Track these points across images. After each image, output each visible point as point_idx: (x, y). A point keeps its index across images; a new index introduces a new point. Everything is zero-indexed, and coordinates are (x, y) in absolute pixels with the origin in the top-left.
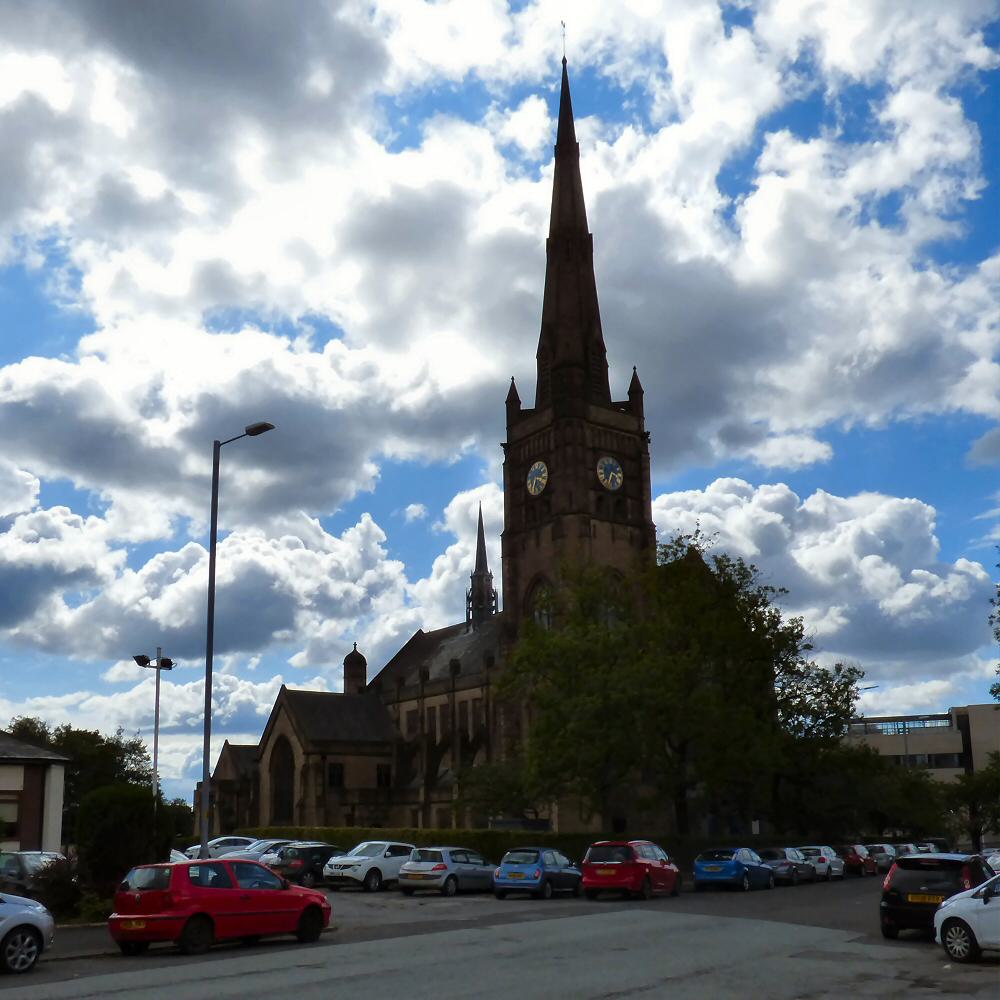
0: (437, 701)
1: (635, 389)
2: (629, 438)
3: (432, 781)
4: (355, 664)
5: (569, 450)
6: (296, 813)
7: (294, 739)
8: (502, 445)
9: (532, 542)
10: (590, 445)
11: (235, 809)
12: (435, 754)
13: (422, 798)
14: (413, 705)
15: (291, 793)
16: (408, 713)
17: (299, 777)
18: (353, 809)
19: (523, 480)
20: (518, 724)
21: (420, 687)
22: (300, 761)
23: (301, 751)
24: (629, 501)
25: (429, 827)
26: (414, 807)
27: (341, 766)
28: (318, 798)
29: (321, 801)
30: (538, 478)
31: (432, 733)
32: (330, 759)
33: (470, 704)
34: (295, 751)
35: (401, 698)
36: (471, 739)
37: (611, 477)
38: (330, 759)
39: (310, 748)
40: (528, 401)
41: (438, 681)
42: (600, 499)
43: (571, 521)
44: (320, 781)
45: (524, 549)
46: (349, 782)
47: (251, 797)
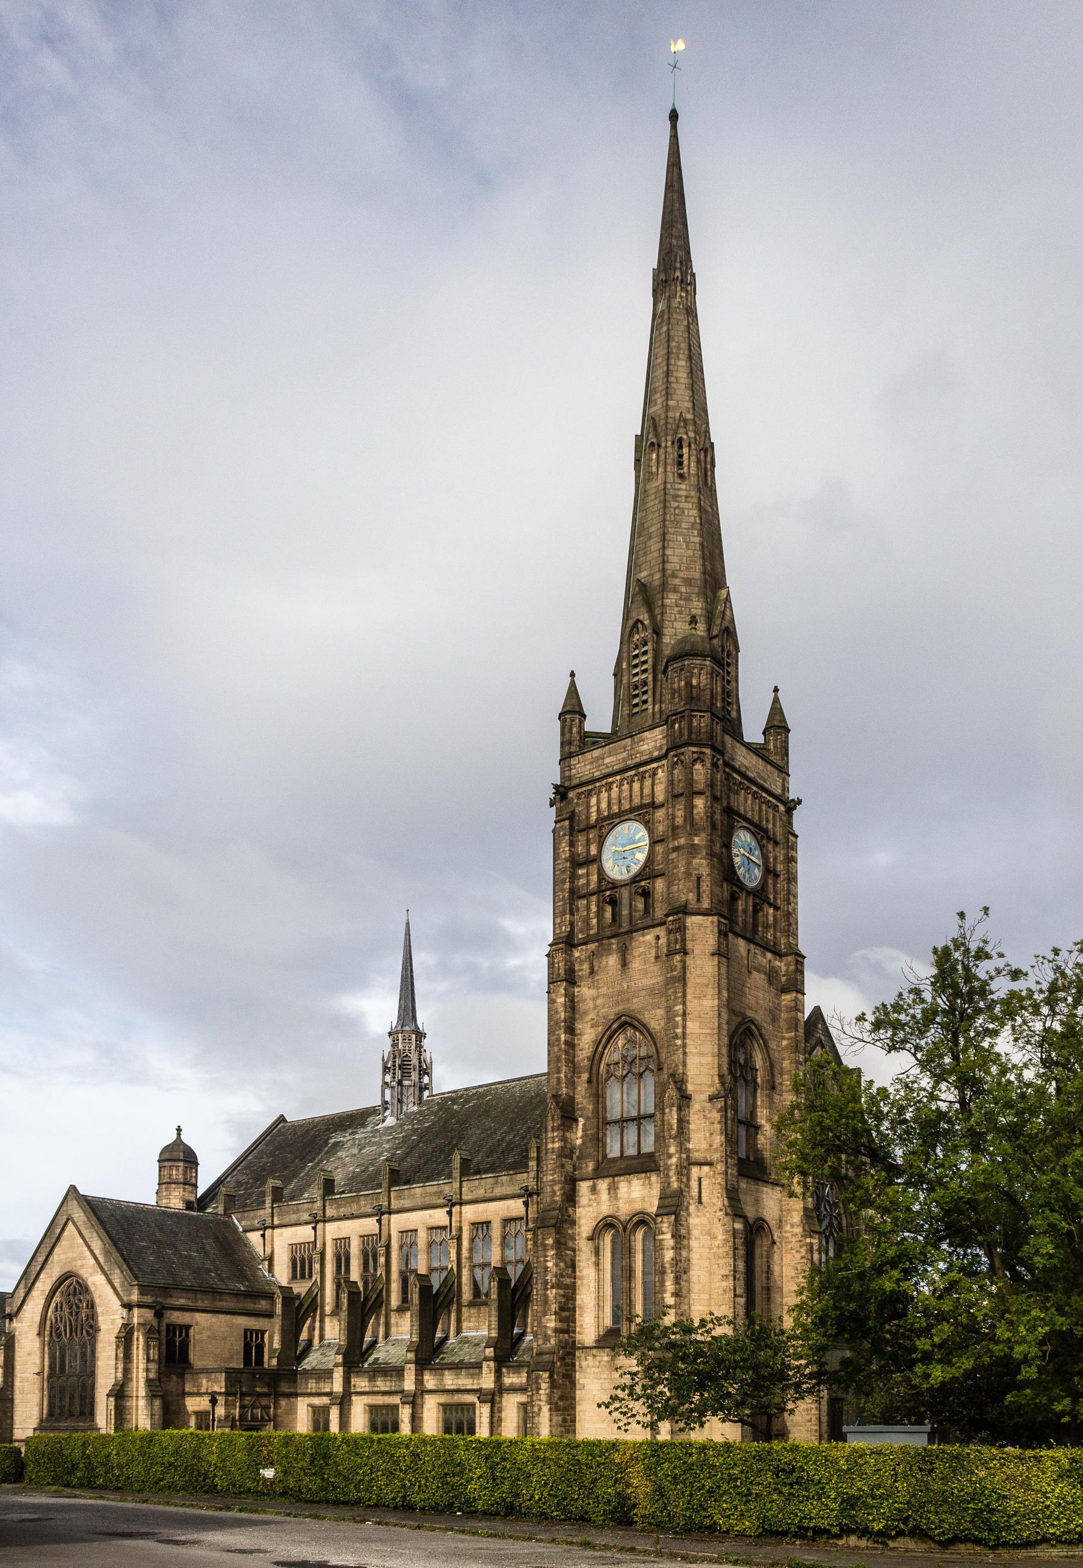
1: (777, 725)
4: (179, 1158)
7: (96, 1282)
9: (612, 961)
13: (337, 1386)
14: (305, 1233)
18: (214, 1402)
19: (593, 851)
20: (573, 1266)
22: (111, 1315)
33: (422, 1237)
35: (276, 1222)
40: (599, 717)
44: (154, 1353)
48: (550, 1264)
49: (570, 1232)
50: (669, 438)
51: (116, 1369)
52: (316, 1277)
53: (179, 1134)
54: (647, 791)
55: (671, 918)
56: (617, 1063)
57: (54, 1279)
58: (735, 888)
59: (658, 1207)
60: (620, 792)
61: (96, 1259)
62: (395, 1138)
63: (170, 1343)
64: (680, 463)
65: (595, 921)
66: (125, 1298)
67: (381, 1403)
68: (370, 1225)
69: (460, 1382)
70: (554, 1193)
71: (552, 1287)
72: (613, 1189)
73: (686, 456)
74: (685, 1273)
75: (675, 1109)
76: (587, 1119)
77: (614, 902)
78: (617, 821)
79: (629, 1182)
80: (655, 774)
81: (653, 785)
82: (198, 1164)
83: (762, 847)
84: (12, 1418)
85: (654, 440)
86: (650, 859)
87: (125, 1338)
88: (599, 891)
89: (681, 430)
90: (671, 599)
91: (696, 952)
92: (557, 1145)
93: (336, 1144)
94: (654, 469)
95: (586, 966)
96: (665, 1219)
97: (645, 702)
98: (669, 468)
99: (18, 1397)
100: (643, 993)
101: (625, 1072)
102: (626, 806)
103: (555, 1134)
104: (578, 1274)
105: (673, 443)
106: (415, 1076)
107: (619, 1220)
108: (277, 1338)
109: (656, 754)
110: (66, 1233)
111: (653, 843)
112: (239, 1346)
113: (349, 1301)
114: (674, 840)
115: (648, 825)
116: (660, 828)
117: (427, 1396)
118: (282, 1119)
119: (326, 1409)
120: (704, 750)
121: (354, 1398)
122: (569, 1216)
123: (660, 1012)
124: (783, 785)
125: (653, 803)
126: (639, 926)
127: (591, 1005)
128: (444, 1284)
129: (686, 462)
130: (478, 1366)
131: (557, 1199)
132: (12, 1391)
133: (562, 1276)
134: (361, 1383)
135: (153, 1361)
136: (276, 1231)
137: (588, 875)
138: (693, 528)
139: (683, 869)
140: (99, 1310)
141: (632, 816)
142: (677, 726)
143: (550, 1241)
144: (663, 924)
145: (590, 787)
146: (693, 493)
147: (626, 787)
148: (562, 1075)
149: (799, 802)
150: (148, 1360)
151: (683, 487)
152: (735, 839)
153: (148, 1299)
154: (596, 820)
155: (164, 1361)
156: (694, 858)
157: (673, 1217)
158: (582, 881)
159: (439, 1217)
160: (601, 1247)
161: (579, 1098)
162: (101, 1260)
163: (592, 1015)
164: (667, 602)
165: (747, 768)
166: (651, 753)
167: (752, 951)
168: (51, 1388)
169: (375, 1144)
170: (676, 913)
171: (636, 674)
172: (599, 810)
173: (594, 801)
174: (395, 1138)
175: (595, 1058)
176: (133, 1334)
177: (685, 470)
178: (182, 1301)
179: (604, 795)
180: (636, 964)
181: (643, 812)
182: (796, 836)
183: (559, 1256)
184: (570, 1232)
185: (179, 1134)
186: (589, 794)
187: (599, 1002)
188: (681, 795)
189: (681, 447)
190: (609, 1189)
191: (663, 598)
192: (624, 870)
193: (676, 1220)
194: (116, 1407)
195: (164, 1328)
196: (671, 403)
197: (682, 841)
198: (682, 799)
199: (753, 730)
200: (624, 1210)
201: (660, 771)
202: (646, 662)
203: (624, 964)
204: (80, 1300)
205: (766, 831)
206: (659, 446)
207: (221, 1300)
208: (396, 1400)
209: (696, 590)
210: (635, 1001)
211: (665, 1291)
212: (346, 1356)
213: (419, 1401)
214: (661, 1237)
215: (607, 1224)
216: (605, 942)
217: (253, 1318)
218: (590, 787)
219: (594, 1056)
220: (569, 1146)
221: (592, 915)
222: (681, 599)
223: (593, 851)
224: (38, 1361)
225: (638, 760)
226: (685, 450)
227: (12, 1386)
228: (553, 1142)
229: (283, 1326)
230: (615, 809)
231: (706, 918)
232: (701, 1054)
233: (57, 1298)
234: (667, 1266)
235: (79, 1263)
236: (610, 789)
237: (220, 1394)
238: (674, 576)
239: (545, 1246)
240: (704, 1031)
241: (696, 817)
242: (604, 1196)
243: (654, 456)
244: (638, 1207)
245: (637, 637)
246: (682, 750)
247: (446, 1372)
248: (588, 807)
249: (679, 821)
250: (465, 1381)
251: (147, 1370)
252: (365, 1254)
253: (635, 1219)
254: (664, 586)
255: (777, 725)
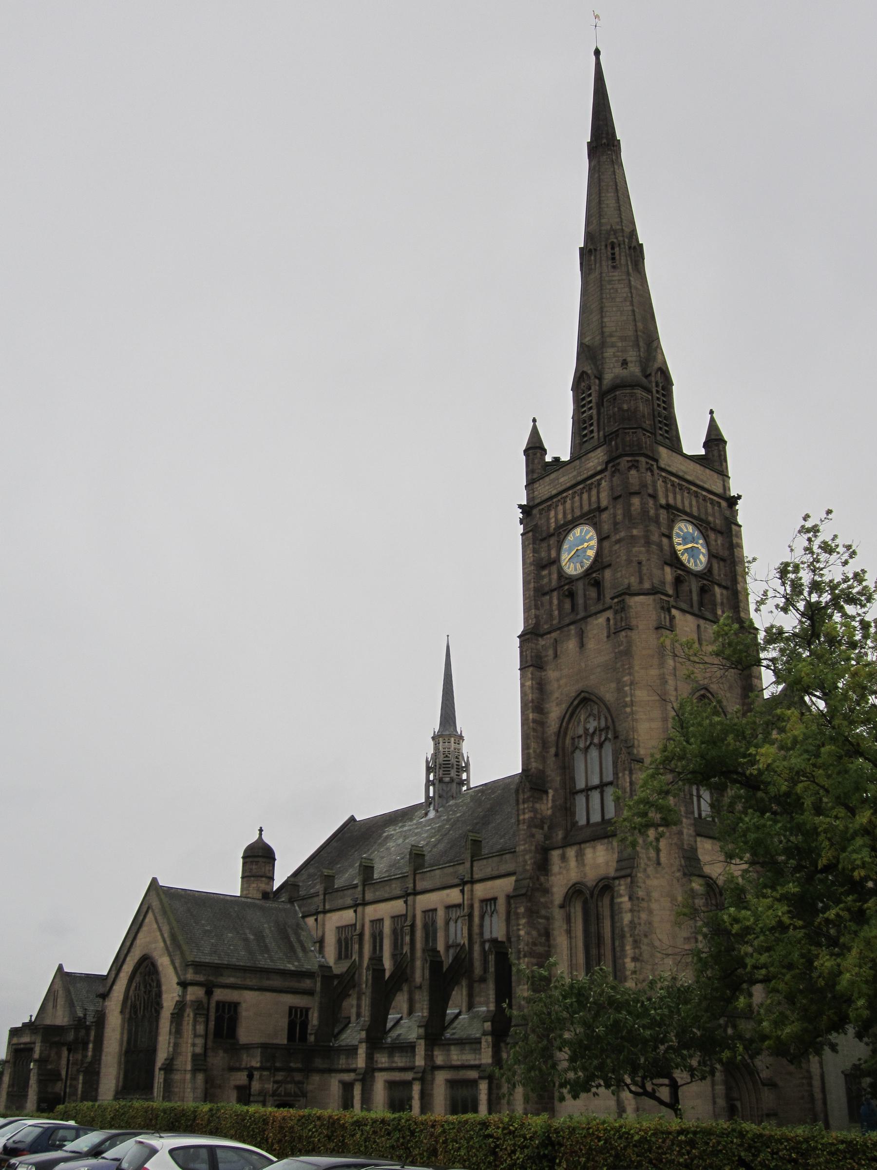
0: (386, 910)
1: (715, 441)
2: (712, 502)
3: (376, 1036)
5: (636, 501)
6: (159, 1077)
7: (164, 962)
8: (520, 506)
9: (571, 645)
10: (663, 501)
11: (64, 1073)
12: (385, 991)
13: (361, 1062)
14: (347, 916)
15: (152, 1051)
16: (339, 929)
17: (168, 1024)
18: (250, 1077)
19: (553, 554)
20: (547, 934)
21: (360, 888)
23: (175, 980)
24: (717, 590)
25: (369, 1110)
26: (348, 1077)
27: (234, 1007)
28: (195, 1056)
29: (200, 1063)
30: (580, 548)
31: (377, 959)
32: (219, 995)
33: (441, 913)
34: (163, 980)
35: (327, 907)
36: (387, 975)
37: (691, 547)
38: (219, 995)
39: (190, 976)
40: (559, 445)
41: (386, 882)
42: (678, 581)
43: (642, 608)
44: (200, 1029)
45: (556, 656)
46: (244, 1035)
47: (90, 1054)
48: (522, 933)
49: (542, 900)
50: (603, 243)
51: (169, 1043)
52: (355, 956)
53: (261, 834)
54: (594, 499)
55: (616, 600)
56: (580, 737)
57: (136, 961)
58: (679, 572)
59: (617, 870)
60: (573, 503)
61: (164, 941)
62: (432, 828)
63: (219, 1019)
64: (613, 259)
65: (556, 613)
66: (182, 977)
67: (398, 1079)
68: (398, 906)
69: (464, 1057)
70: (525, 861)
71: (525, 956)
72: (580, 855)
73: (617, 253)
74: (646, 936)
75: (627, 772)
76: (556, 790)
77: (571, 595)
78: (570, 527)
79: (594, 848)
80: (599, 484)
81: (598, 493)
82: (275, 859)
83: (706, 538)
84: (97, 1090)
85: (592, 247)
86: (598, 554)
87: (177, 1016)
88: (559, 588)
89: (612, 237)
90: (609, 352)
91: (641, 627)
92: (527, 816)
93: (387, 837)
94: (593, 266)
95: (551, 652)
96: (622, 882)
97: (592, 432)
98: (604, 263)
99: (103, 1070)
100: (599, 670)
101: (588, 743)
102: (578, 513)
103: (526, 806)
104: (552, 942)
105: (606, 246)
106: (453, 773)
107: (586, 886)
108: (316, 1015)
109: (599, 468)
110: (147, 920)
111: (601, 540)
112: (284, 1023)
113: (373, 977)
114: (616, 534)
115: (596, 526)
116: (606, 527)
117: (376, 1074)
118: (352, 819)
119: (408, 1084)
120: (637, 458)
121: (376, 1074)
122: (541, 884)
123: (613, 685)
124: (724, 485)
125: (599, 507)
126: (593, 612)
127: (556, 685)
128: (456, 958)
129: (617, 257)
130: (478, 1041)
131: (528, 868)
132: (100, 1064)
133: (534, 944)
134: (382, 1060)
135: (200, 1036)
136: (328, 915)
137: (550, 574)
138: (625, 301)
139: (624, 558)
140: (164, 988)
141: (582, 521)
142: (613, 443)
143: (521, 910)
144: (610, 608)
145: (549, 503)
146: (624, 277)
147: (577, 498)
148: (531, 751)
149: (739, 497)
150: (196, 1036)
151: (616, 274)
152: (676, 530)
153: (201, 978)
154: (554, 529)
155: (211, 1036)
156: (634, 547)
157: (629, 880)
158: (546, 581)
159: (454, 896)
160: (572, 915)
161: (549, 772)
162: (168, 942)
163: (556, 695)
164: (606, 355)
165: (685, 473)
166: (595, 468)
167: (702, 626)
168: (127, 1062)
169: (416, 834)
170: (620, 595)
171: (584, 412)
172: (556, 520)
173: (552, 513)
174: (432, 828)
175: (561, 733)
176: (184, 1010)
177: (618, 262)
178: (231, 980)
179: (560, 507)
180: (591, 645)
181: (591, 517)
182: (740, 526)
183: (531, 924)
184: (542, 900)
185: (261, 834)
186: (549, 508)
187: (562, 682)
188: (620, 496)
189: (613, 248)
190: (577, 857)
191: (602, 353)
192: (578, 565)
193: (632, 882)
194: (165, 1080)
195: (213, 1005)
196: (603, 221)
197: (623, 534)
198: (621, 500)
199: (693, 443)
200: (591, 875)
201: (603, 481)
202: (590, 402)
203: (582, 645)
204: (152, 980)
205: (708, 523)
206: (595, 250)
207: (268, 979)
208: (409, 1076)
209: (631, 344)
210: (591, 677)
211: (625, 956)
212: (368, 1031)
213: (429, 1077)
214: (619, 900)
215: (576, 891)
216: (566, 629)
217: (298, 996)
218: (549, 503)
219: (559, 731)
220: (539, 816)
221: (554, 607)
222: (618, 351)
223: (553, 554)
224: (118, 1037)
225: (585, 476)
226: (617, 250)
227: (100, 1060)
228: (524, 813)
229: (321, 1003)
230: (569, 517)
231: (647, 597)
232: (651, 720)
233: (137, 979)
234: (626, 929)
235: (153, 946)
236: (565, 502)
237: (256, 1069)
238: (611, 336)
239: (517, 914)
240: (653, 698)
241: (634, 513)
242: (573, 863)
243: (593, 258)
244: (602, 872)
245: (583, 384)
246: (618, 461)
247: (452, 1048)
248: (548, 519)
249: (619, 518)
250: (468, 1058)
251: (194, 1045)
252: (394, 932)
253: (601, 885)
254: (603, 344)
255: (715, 441)
